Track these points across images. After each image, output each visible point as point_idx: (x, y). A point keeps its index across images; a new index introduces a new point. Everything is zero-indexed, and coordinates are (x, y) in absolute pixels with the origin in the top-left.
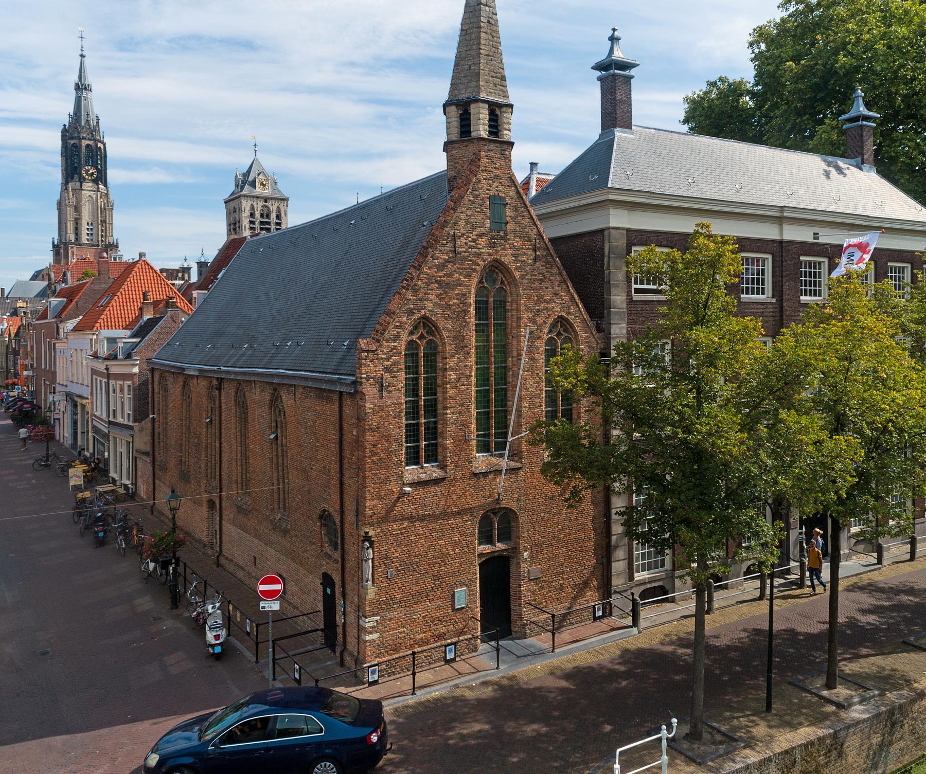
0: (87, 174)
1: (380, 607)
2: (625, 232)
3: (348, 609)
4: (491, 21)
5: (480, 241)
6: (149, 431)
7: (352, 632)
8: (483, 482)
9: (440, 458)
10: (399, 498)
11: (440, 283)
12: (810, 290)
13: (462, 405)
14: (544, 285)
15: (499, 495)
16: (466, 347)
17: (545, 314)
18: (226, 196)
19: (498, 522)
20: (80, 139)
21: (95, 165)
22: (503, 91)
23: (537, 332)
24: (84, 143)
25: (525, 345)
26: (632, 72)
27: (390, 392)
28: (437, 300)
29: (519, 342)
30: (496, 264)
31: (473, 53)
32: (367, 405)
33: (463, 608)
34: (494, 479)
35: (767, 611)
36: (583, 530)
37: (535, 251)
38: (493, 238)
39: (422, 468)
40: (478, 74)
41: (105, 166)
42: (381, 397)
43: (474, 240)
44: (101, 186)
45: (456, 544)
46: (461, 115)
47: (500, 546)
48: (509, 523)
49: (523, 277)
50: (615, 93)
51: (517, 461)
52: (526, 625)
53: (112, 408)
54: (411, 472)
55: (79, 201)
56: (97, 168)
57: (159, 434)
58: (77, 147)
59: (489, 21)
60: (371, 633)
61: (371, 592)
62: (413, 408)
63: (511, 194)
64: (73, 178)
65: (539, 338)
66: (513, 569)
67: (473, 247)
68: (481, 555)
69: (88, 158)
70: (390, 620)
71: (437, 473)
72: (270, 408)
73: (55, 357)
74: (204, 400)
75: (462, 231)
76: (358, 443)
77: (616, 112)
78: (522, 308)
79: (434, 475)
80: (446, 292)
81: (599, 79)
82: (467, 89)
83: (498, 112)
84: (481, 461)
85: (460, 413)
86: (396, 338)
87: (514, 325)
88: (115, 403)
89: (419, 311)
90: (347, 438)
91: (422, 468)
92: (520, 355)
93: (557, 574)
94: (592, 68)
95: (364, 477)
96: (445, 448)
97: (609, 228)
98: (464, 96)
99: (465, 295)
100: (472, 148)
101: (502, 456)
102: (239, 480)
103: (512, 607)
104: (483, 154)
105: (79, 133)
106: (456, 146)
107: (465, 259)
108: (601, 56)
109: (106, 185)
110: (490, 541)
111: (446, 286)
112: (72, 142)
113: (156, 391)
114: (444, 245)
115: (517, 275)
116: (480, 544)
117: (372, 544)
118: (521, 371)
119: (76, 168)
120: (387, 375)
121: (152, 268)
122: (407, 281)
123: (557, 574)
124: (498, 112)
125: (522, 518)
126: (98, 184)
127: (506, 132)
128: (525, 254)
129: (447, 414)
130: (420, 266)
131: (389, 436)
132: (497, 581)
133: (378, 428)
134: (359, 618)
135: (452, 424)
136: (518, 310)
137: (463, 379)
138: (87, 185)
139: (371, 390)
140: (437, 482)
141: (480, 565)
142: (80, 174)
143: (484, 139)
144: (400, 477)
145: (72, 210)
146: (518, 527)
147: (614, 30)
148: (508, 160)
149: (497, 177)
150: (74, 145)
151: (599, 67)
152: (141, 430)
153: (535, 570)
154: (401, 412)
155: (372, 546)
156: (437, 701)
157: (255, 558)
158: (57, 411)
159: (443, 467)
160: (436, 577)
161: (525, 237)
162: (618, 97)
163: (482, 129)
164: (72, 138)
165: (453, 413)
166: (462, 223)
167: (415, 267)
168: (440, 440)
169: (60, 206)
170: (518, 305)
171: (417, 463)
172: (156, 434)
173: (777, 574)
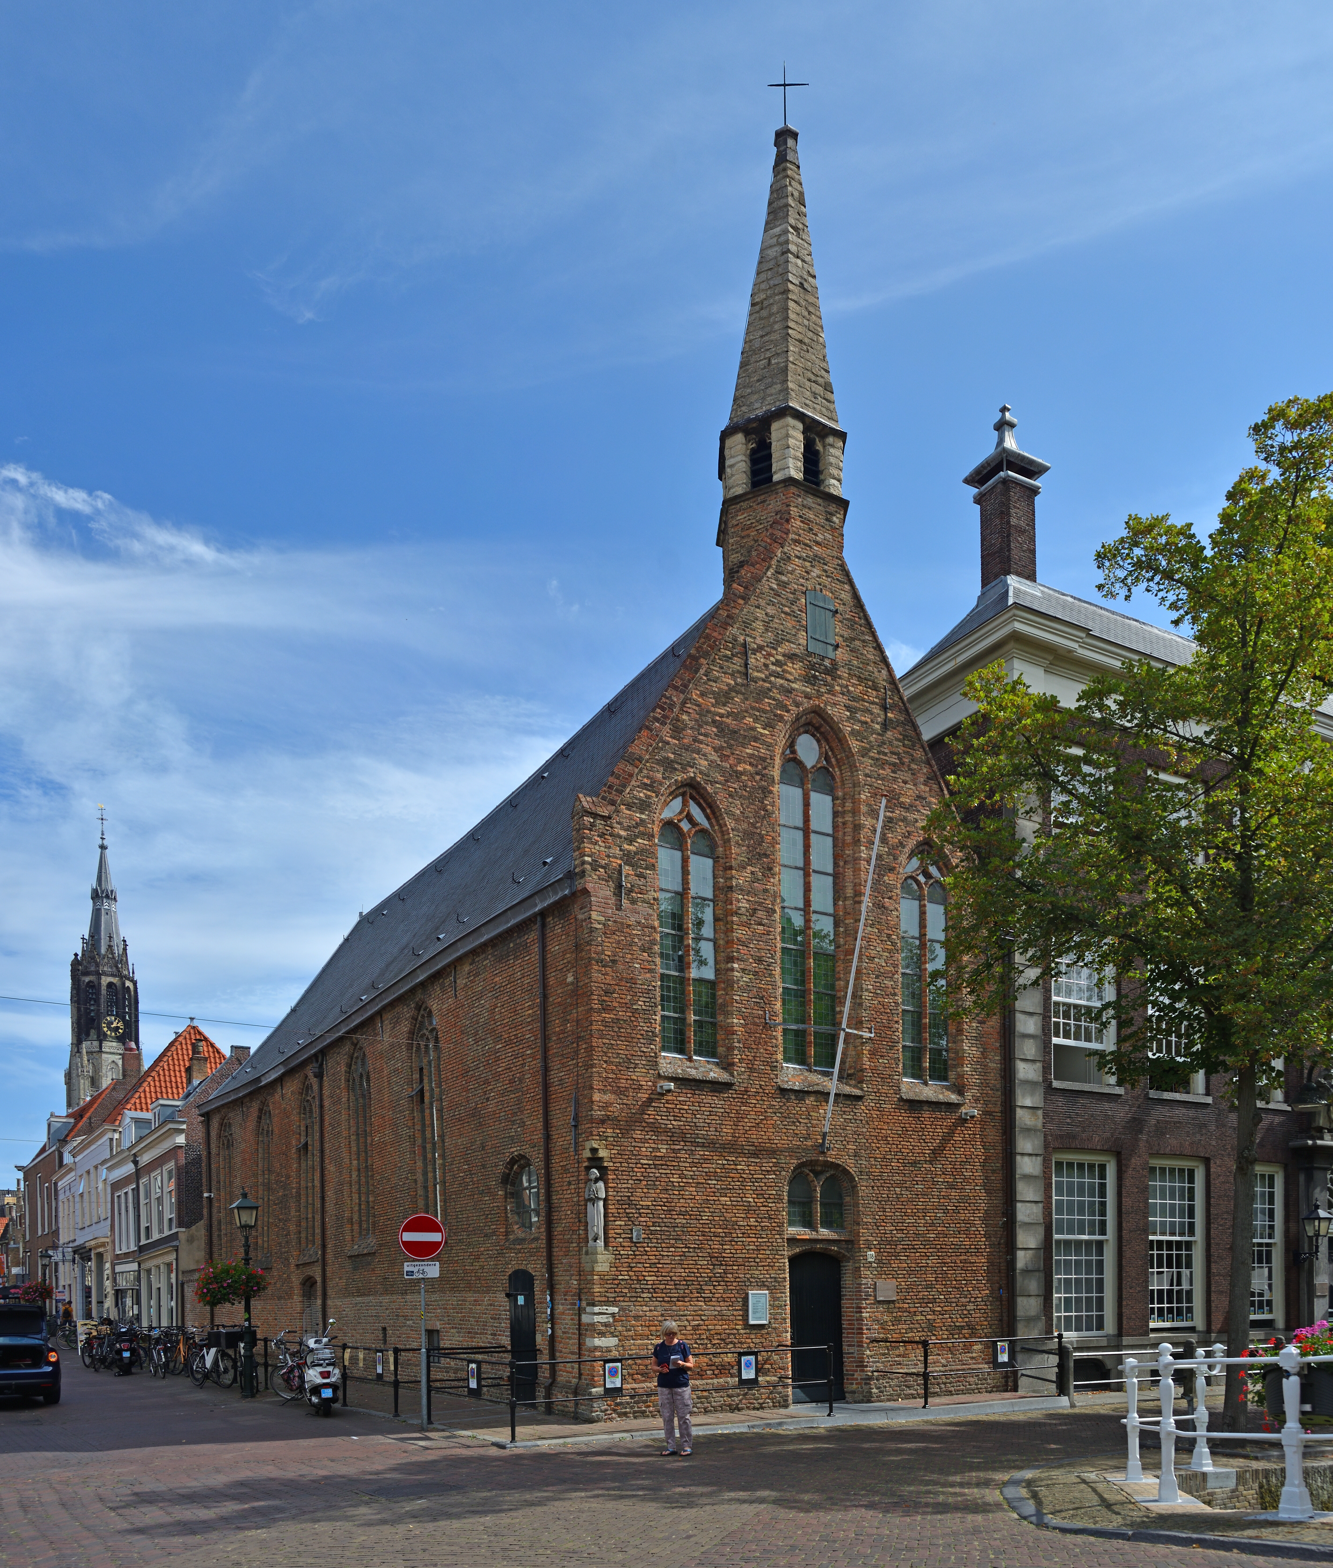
0: (109, 1028)
1: (620, 1290)
2: (1000, 485)
3: (560, 1308)
4: (806, 285)
5: (789, 667)
6: (202, 1242)
7: (567, 1347)
8: (795, 1107)
9: (721, 1050)
10: (650, 1100)
11: (722, 729)
12: (1160, 1301)
14: (901, 775)
15: (824, 1135)
17: (901, 828)
18: (26, 1161)
19: (822, 1186)
20: (99, 975)
21: (120, 1016)
22: (828, 409)
23: (888, 859)
24: (105, 980)
25: (869, 876)
27: (633, 902)
28: (714, 757)
29: (857, 870)
30: (817, 720)
31: (774, 337)
32: (594, 915)
33: (762, 1326)
34: (816, 1108)
35: (1213, 1265)
36: (967, 1232)
37: (885, 708)
38: (812, 667)
39: (690, 1059)
40: (785, 370)
41: (137, 1016)
42: (619, 907)
43: (778, 663)
45: (749, 1210)
46: (753, 452)
47: (824, 1233)
48: (841, 1197)
49: (864, 753)
50: (1009, 515)
51: (855, 1087)
52: (870, 1378)
53: (144, 1224)
54: (670, 1062)
55: (97, 1069)
57: (219, 1222)
58: (94, 987)
59: (801, 285)
60: (602, 1334)
61: (603, 1262)
62: (675, 1030)
63: (843, 595)
64: (88, 1035)
65: (892, 869)
66: (847, 1280)
68: (792, 1241)
69: (110, 1003)
70: (637, 1318)
71: (715, 1074)
72: (410, 1047)
73: (56, 1208)
74: (295, 1117)
75: (759, 641)
76: (579, 993)
77: (1005, 548)
78: (864, 808)
79: (712, 1074)
81: (978, 500)
82: (764, 398)
84: (792, 1074)
85: (756, 974)
86: (644, 806)
87: (848, 839)
88: (149, 1219)
89: (684, 770)
91: (690, 1059)
92: (858, 894)
93: (925, 1302)
94: (1047, 469)
95: (590, 1049)
96: (730, 1032)
98: (760, 410)
99: (764, 759)
100: (774, 503)
101: (828, 1074)
102: (356, 1217)
103: (845, 1348)
104: (794, 511)
105: (97, 965)
106: (744, 505)
107: (765, 693)
108: (985, 451)
110: (808, 1223)
111: (732, 737)
112: (87, 979)
113: (214, 1151)
114: (728, 659)
115: (854, 745)
116: (791, 1223)
117: (603, 1170)
118: (861, 924)
119: (92, 1020)
120: (627, 869)
121: (219, 1052)
122: (663, 709)
123: (925, 1302)
124: (819, 447)
125: (863, 1190)
127: (833, 481)
128: (868, 711)
129: (732, 970)
130: (686, 686)
131: (633, 981)
132: (819, 1285)
133: (614, 962)
134: (580, 1311)
135: (743, 990)
136: (855, 812)
137: (760, 914)
138: (111, 1045)
139: (600, 891)
140: (717, 1087)
141: (792, 1260)
144: (653, 1063)
145: (88, 1083)
146: (856, 1205)
148: (838, 533)
149: (816, 559)
150: (90, 985)
151: (978, 478)
152: (191, 1240)
153: (887, 1289)
154: (653, 942)
156: (731, 1490)
157: (384, 1329)
158: (61, 1289)
159: (727, 1066)
160: (716, 1259)
162: (1014, 521)
164: (86, 973)
165: (743, 970)
166: (759, 625)
167: (676, 688)
168: (721, 1018)
169: (69, 1076)
170: (856, 802)
171: (681, 1051)
172: (215, 1223)
173: (1112, 1386)
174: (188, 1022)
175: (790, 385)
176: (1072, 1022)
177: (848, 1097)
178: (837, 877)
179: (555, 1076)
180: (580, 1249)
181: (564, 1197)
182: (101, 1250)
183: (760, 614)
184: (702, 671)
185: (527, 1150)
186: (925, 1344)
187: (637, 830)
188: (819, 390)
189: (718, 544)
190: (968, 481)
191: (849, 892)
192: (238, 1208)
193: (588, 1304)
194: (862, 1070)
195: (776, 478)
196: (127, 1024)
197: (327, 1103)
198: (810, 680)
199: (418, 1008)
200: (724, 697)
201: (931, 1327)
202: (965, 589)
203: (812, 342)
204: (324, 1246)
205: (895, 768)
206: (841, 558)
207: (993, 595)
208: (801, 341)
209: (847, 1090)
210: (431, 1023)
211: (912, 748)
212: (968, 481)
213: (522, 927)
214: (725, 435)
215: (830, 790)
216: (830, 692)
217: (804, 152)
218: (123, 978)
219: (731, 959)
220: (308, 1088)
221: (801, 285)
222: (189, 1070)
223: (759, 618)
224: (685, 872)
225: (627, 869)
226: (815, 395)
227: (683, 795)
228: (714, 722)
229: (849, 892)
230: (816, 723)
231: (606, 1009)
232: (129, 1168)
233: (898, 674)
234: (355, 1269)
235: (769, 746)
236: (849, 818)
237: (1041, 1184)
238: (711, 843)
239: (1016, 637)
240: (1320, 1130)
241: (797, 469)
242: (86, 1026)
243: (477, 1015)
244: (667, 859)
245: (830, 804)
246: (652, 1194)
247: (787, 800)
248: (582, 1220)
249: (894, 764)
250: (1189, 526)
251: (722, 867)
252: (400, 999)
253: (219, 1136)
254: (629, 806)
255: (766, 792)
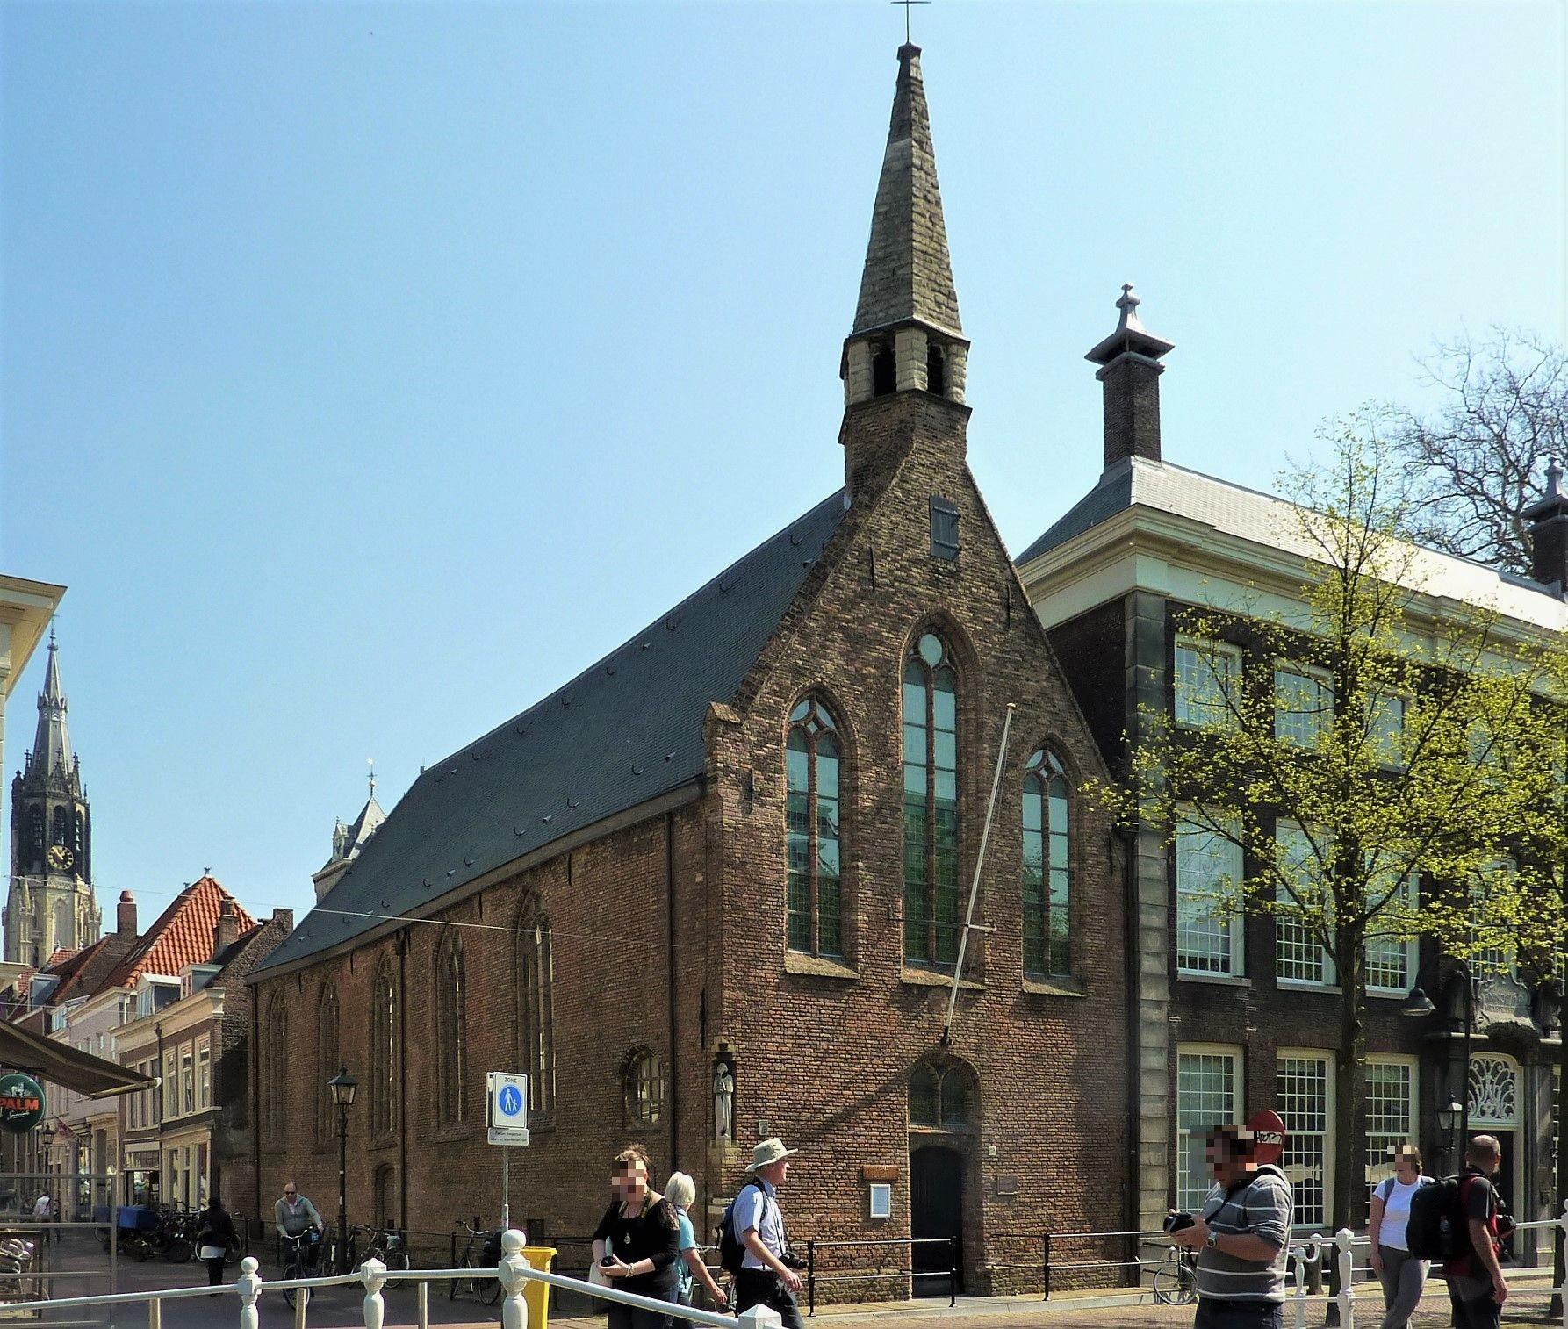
2: (1162, 600)
4: (930, 197)
11: (849, 636)
13: (884, 858)
16: (890, 756)
18: (318, 867)
21: (69, 844)
24: (52, 804)
26: (1162, 360)
27: (763, 805)
29: (979, 767)
32: (725, 819)
37: (1008, 609)
41: (88, 846)
43: (902, 568)
44: (80, 883)
54: (797, 961)
55: (40, 907)
56: (73, 849)
58: (40, 811)
59: (925, 197)
64: (30, 867)
67: (902, 580)
69: (56, 827)
76: (709, 893)
77: (1131, 425)
78: (986, 705)
80: (856, 650)
83: (943, 354)
86: (774, 712)
90: (685, 893)
93: (1046, 1196)
97: (1136, 591)
100: (899, 412)
107: (888, 598)
108: (1106, 329)
109: (88, 881)
111: (858, 642)
112: (32, 802)
115: (978, 645)
117: (732, 1067)
120: (757, 774)
123: (1046, 1196)
126: (74, 879)
129: (857, 868)
131: (761, 882)
132: (942, 1188)
133: (744, 863)
136: (977, 710)
139: (730, 796)
140: (841, 984)
142: (44, 860)
143: (914, 392)
144: (780, 959)
146: (977, 1099)
147: (1127, 288)
155: (731, 1071)
161: (989, 580)
163: (917, 379)
164: (32, 795)
172: (262, 1102)
174: (203, 874)
175: (915, 297)
176: (956, 982)
177: (970, 991)
178: (959, 774)
179: (682, 971)
180: (707, 1143)
181: (692, 1088)
182: (103, 1127)
183: (885, 522)
184: (829, 579)
185: (650, 1041)
186: (1046, 1238)
187: (766, 736)
188: (941, 298)
189: (276, 911)
190: (1093, 356)
191: (972, 789)
192: (337, 1084)
193: (716, 1196)
194: (984, 964)
195: (898, 388)
196: (77, 855)
197: (409, 983)
198: (935, 583)
199: (525, 892)
200: (849, 604)
201: (1052, 1221)
202: (1087, 471)
203: (938, 258)
204: (404, 1131)
205: (1018, 666)
206: (963, 463)
207: (1115, 476)
208: (925, 253)
209: (970, 985)
210: (538, 908)
211: (1035, 645)
212: (1093, 356)
213: (647, 824)
214: (847, 343)
215: (953, 689)
216: (952, 594)
217: (927, 69)
218: (73, 801)
219: (856, 858)
220: (383, 964)
221: (925, 197)
222: (216, 931)
223: (887, 525)
224: (811, 774)
225: (757, 774)
226: (938, 304)
227: (810, 699)
228: (841, 627)
229: (972, 789)
230: (942, 626)
231: (736, 909)
232: (150, 1037)
233: (1014, 553)
234: (442, 1155)
235: (895, 649)
236: (971, 716)
237: (1165, 1124)
238: (839, 746)
239: (1138, 534)
240: (1457, 1021)
241: (923, 379)
242: (28, 857)
243: (595, 905)
244: (794, 762)
245: (953, 702)
246: (778, 1087)
247: (910, 700)
248: (710, 1115)
249: (1016, 662)
250: (1163, 348)
251: (848, 770)
252: (506, 882)
253: (269, 1009)
254: (759, 713)
255: (891, 694)
